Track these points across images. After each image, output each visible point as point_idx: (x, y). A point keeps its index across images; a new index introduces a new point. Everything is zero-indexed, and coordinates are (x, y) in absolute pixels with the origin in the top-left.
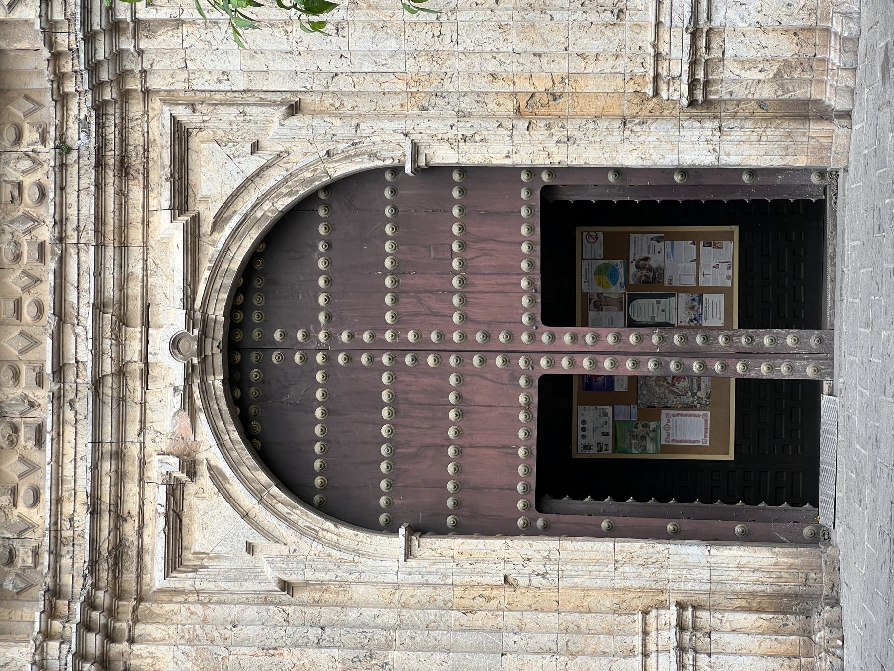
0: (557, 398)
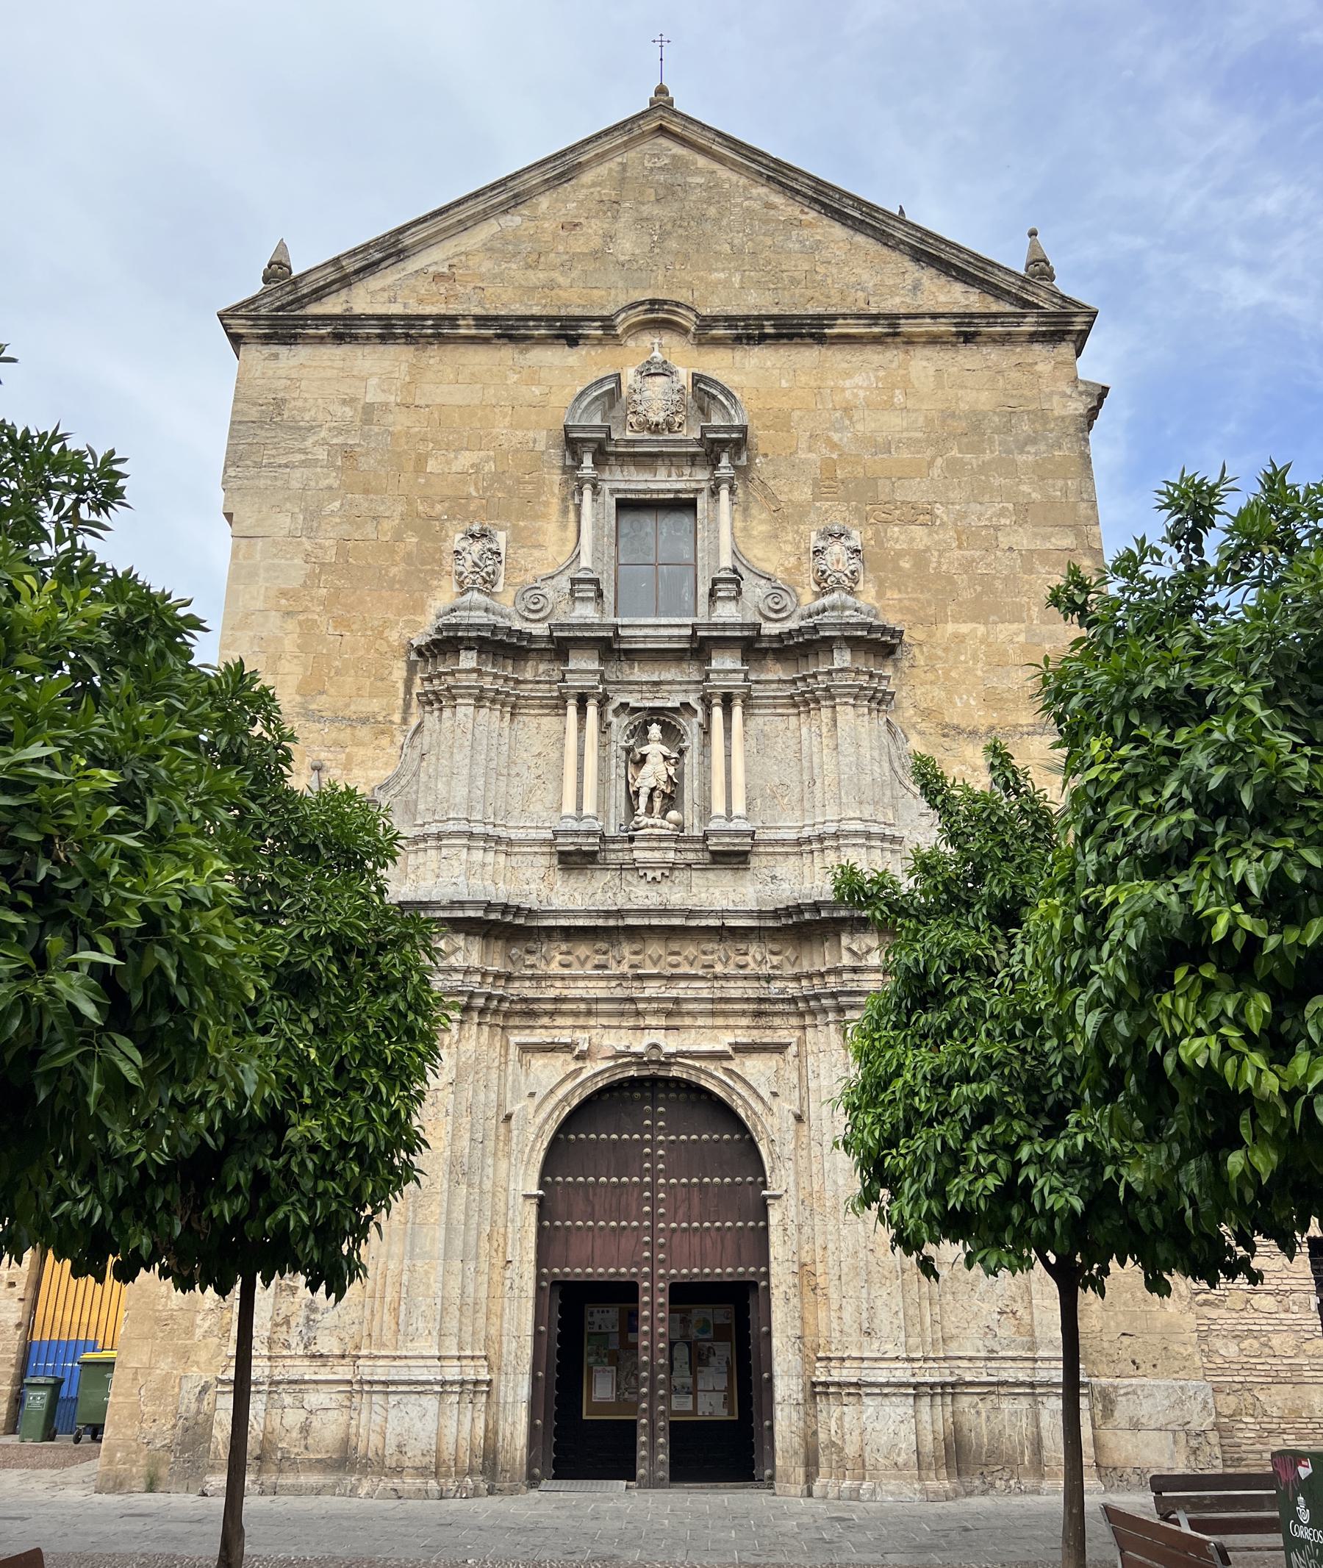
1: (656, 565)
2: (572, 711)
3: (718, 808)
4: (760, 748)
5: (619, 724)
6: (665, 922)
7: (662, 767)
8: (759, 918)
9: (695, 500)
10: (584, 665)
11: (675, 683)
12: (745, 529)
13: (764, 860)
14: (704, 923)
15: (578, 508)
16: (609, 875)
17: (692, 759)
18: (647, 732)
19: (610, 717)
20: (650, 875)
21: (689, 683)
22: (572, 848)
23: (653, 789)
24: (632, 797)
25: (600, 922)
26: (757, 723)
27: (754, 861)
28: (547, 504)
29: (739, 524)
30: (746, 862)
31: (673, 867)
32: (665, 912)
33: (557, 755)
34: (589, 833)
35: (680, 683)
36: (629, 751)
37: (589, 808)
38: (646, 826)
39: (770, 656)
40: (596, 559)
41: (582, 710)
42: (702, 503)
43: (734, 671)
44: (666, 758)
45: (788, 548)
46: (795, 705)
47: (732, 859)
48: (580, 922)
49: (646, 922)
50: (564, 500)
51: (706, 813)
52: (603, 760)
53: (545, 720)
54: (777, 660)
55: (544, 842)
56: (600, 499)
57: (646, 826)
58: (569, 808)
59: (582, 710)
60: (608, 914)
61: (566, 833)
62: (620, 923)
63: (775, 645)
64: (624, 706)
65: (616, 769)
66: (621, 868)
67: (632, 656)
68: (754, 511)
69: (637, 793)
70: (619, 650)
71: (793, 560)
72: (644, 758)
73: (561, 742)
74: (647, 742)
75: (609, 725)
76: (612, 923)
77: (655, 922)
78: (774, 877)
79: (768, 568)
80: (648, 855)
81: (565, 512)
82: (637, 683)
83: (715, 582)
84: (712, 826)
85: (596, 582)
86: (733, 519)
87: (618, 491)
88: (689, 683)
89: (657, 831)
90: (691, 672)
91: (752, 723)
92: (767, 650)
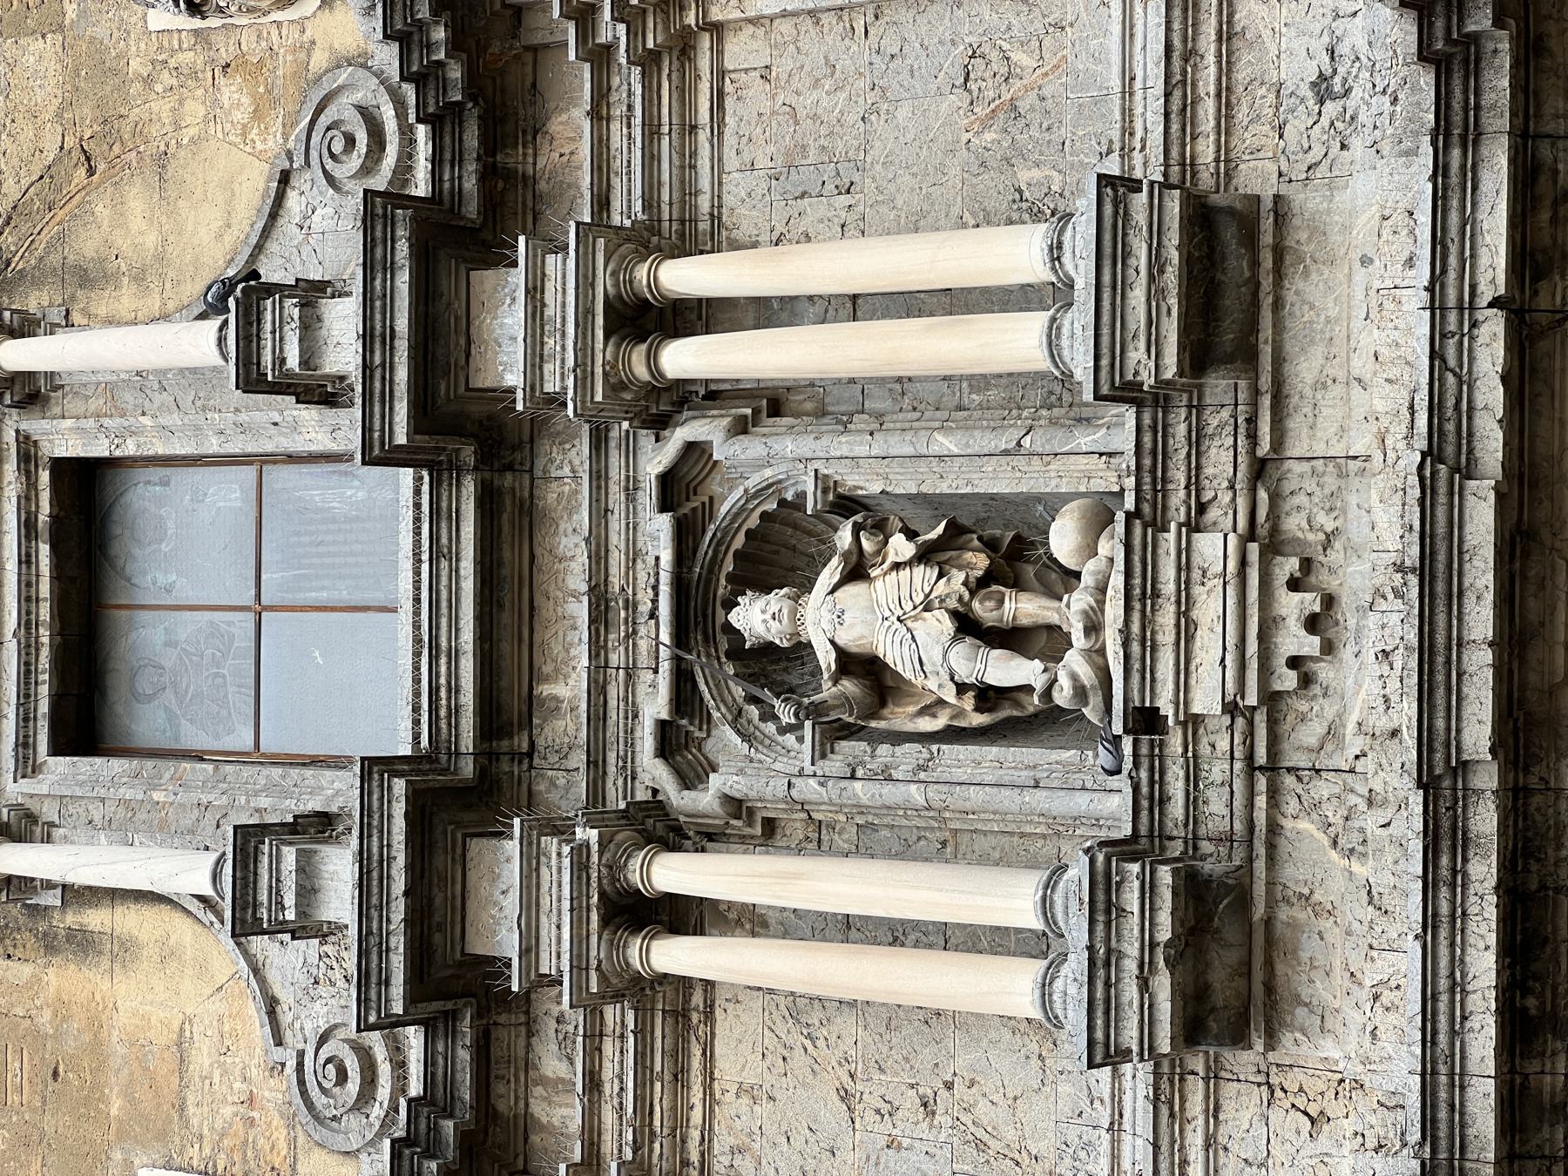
0: (364, 463)
1: (259, 610)
2: (673, 955)
3: (1016, 342)
4: (837, 190)
5: (740, 766)
6: (1481, 574)
7: (885, 588)
8: (1472, 138)
9: (61, 467)
10: (520, 900)
11: (608, 532)
12: (139, 278)
13: (1252, 135)
14: (1491, 395)
15: (75, 895)
16: (1301, 828)
17: (867, 462)
18: (767, 649)
19: (704, 801)
20: (1295, 640)
21: (599, 477)
22: (1163, 984)
23: (966, 625)
24: (1005, 717)
25: (1484, 871)
26: (743, 195)
27: (1257, 178)
28: (62, 1009)
29: (125, 300)
30: (1247, 216)
31: (1265, 538)
32: (1434, 571)
33: (847, 1025)
34: (1103, 902)
35: (600, 513)
36: (834, 733)
37: (1012, 900)
38: (1097, 655)
39: (515, 158)
40: (167, 831)
41: (683, 915)
42: (65, 438)
43: (535, 292)
44: (856, 571)
45: (195, 110)
46: (684, 47)
47: (1221, 277)
48: (1483, 966)
49: (1480, 663)
50: (50, 945)
51: (1038, 397)
52: (873, 837)
53: (728, 1068)
54: (536, 131)
55: (1167, 1103)
56: (49, 812)
57: (1097, 655)
58: (1011, 986)
59: (683, 915)
60: (1443, 838)
61: (1102, 1005)
62: (1487, 778)
63: (472, 139)
64: (670, 742)
65: (895, 779)
66: (1267, 769)
67: (507, 707)
68: (86, 245)
69: (988, 696)
70: (486, 754)
71: (232, 92)
72: (853, 663)
73: (800, 1008)
74: (801, 651)
75: (736, 806)
76: (1485, 820)
77: (1481, 620)
78: (1323, 88)
79: (255, 183)
80: (1208, 648)
81: (83, 944)
82: (598, 689)
83: (252, 380)
84: (1081, 364)
85: (248, 841)
86: (111, 322)
87: (24, 744)
88: (599, 477)
89: (1114, 611)
90: (567, 466)
91: (744, 215)
92: (489, 173)
